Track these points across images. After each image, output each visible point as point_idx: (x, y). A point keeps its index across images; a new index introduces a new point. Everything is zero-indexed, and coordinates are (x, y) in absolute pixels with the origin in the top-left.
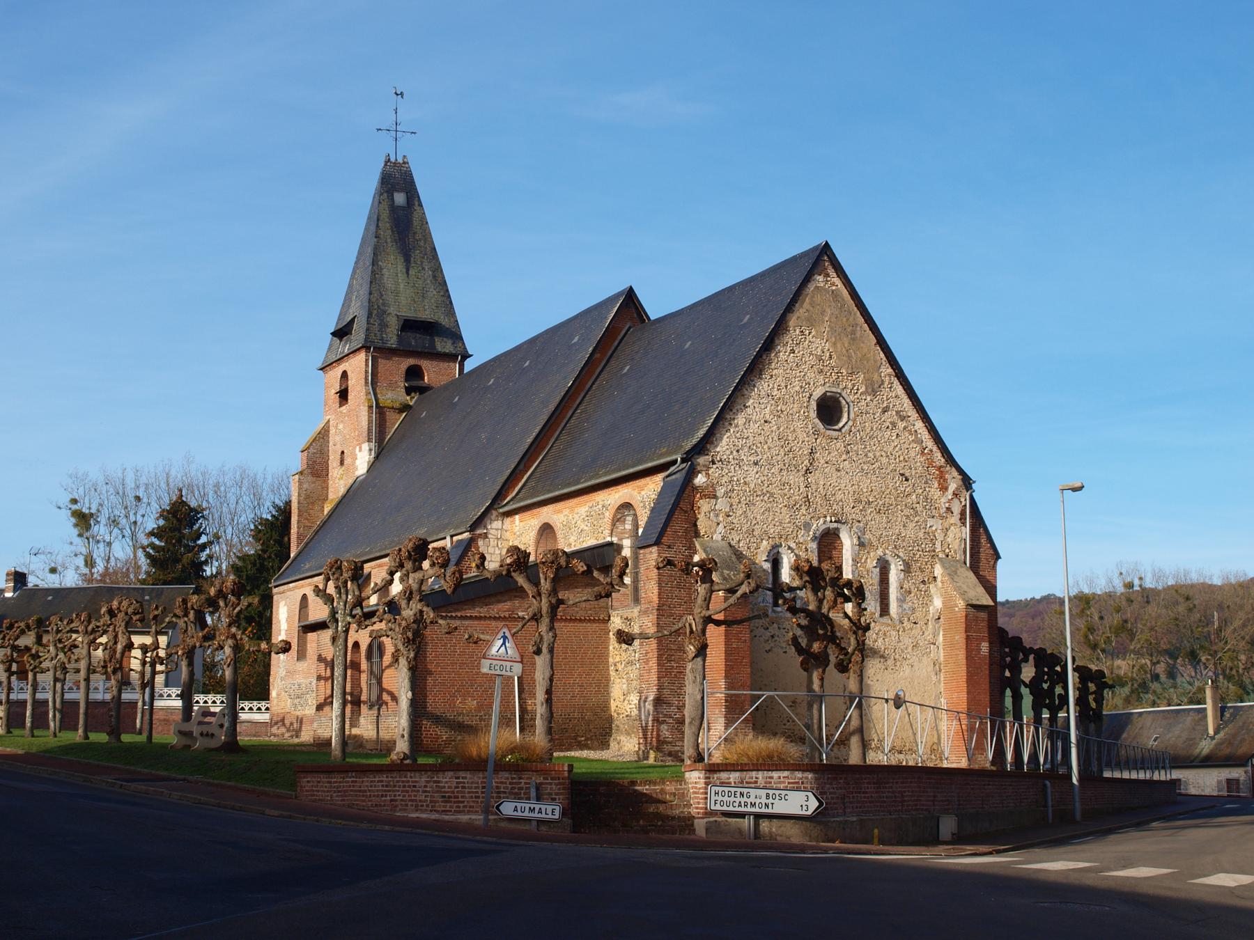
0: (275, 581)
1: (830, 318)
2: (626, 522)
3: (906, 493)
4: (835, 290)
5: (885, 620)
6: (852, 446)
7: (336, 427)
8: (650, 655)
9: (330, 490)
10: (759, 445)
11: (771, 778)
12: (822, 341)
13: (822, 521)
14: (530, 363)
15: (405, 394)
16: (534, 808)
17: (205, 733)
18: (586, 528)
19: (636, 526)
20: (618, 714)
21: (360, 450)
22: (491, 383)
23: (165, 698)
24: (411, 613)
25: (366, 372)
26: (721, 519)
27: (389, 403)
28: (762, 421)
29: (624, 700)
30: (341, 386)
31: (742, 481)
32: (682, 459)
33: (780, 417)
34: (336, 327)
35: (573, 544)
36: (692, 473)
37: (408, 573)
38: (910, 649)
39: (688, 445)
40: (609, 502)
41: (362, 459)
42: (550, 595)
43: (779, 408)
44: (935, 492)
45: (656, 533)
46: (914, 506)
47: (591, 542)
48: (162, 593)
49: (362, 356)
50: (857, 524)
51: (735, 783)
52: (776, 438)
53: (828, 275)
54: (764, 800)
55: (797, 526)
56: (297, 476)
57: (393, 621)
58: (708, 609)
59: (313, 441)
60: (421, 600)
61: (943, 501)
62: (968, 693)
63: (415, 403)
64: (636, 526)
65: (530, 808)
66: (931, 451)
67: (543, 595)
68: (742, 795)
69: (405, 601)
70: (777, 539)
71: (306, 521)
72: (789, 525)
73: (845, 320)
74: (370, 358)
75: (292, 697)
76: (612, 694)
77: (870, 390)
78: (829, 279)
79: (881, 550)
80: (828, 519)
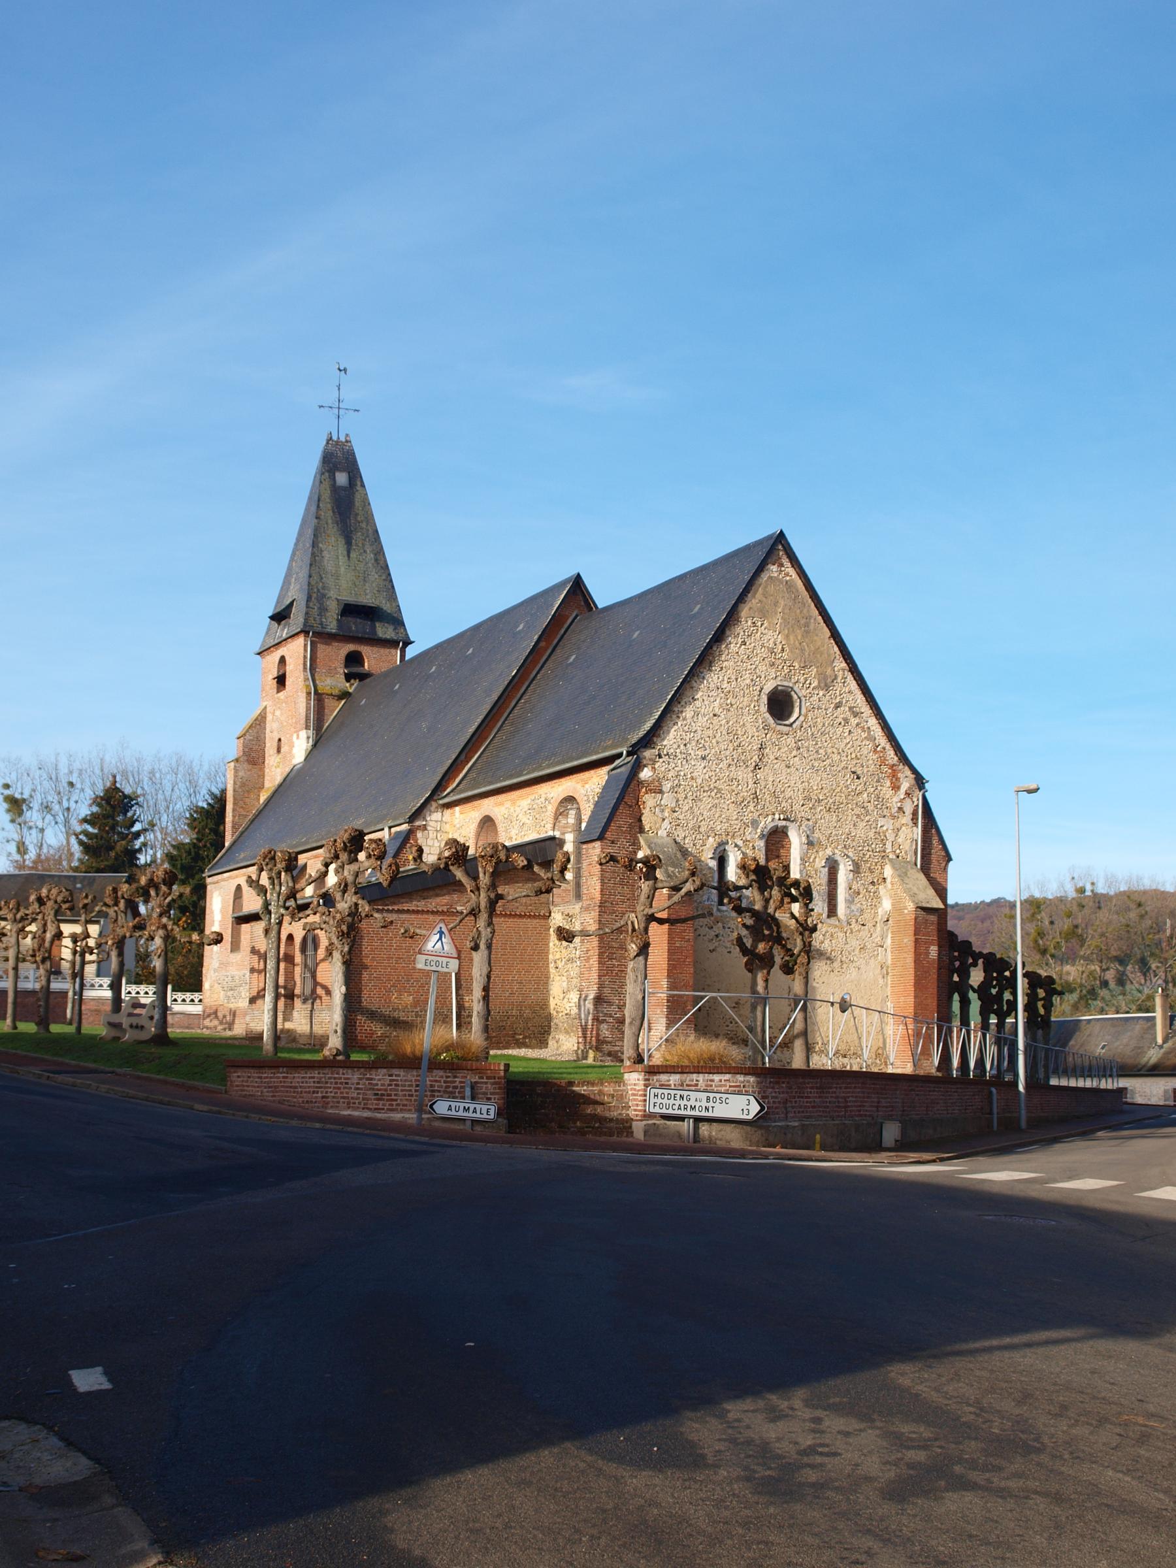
1: (783, 609)
3: (857, 792)
4: (789, 580)
5: (833, 921)
6: (803, 742)
8: (591, 953)
10: (707, 739)
13: (770, 818)
15: (344, 681)
16: (469, 1108)
17: (134, 1024)
19: (579, 820)
20: (557, 1012)
21: (298, 738)
22: (433, 670)
24: (346, 906)
25: (305, 657)
26: (666, 814)
28: (711, 715)
29: (564, 998)
30: (278, 671)
31: (689, 776)
32: (628, 752)
34: (275, 608)
36: (638, 766)
37: (344, 865)
38: (857, 952)
40: (552, 795)
41: (299, 747)
43: (729, 701)
46: (865, 805)
48: (94, 880)
50: (807, 822)
51: (675, 1085)
52: (724, 732)
53: (781, 565)
54: (704, 1104)
55: (744, 823)
56: (232, 764)
57: (327, 913)
59: (249, 728)
61: (895, 801)
62: (915, 997)
63: (355, 690)
64: (579, 820)
65: (464, 1107)
66: (884, 748)
67: (482, 890)
68: (682, 1097)
69: (340, 893)
70: (724, 836)
73: (798, 611)
75: (225, 989)
77: (822, 685)
78: (783, 569)
80: (777, 816)
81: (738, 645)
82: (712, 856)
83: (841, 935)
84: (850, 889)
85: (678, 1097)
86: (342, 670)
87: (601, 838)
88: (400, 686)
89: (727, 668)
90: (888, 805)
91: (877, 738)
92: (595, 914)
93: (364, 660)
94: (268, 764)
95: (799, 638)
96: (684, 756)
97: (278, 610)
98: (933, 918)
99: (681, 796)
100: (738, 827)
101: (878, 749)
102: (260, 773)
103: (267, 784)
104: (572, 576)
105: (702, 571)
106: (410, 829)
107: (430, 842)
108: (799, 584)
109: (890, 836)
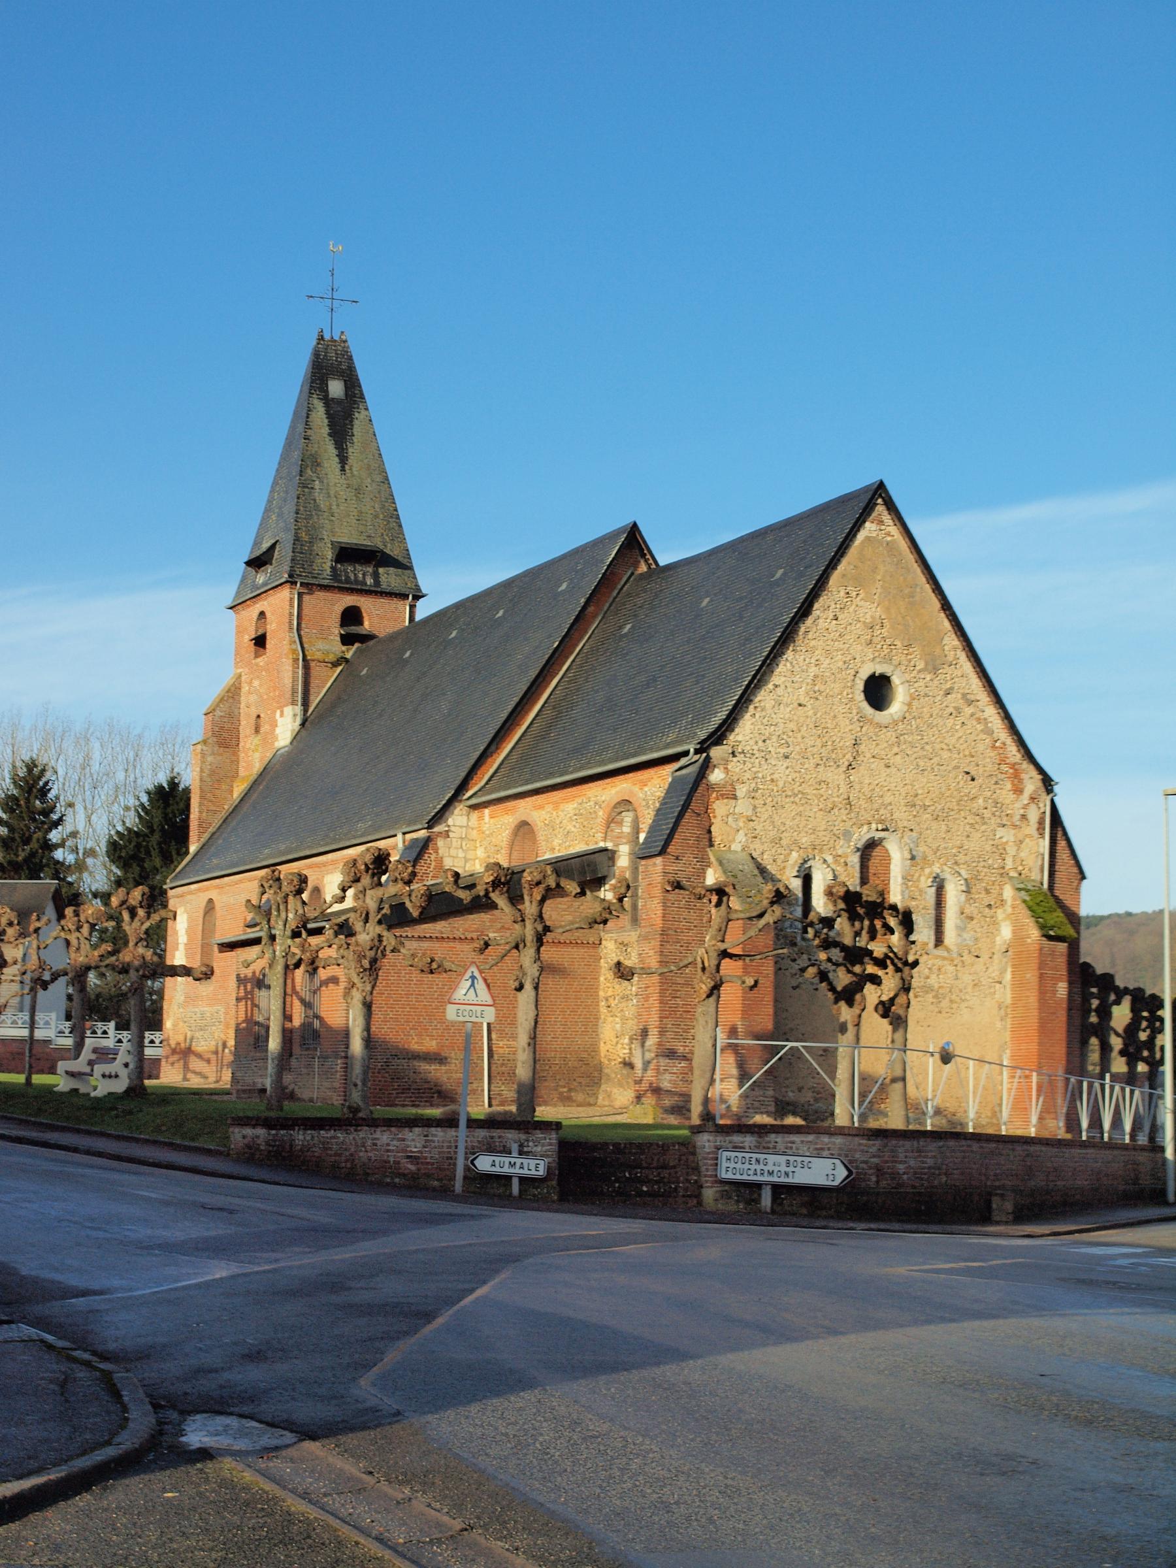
0: (171, 881)
2: (624, 824)
3: (972, 796)
4: (891, 541)
5: (940, 952)
7: (250, 683)
8: (650, 990)
9: (242, 764)
10: (791, 734)
11: (793, 1142)
12: (872, 606)
13: (865, 828)
14: (504, 613)
15: (340, 644)
17: (107, 1073)
18: (573, 829)
19: (636, 830)
20: (609, 1060)
21: (282, 715)
22: (453, 635)
23: (99, 1035)
24: (368, 938)
25: (291, 614)
26: (741, 824)
27: (318, 655)
28: (796, 704)
29: (617, 1043)
30: (257, 631)
31: (769, 778)
32: (695, 749)
33: (817, 699)
34: (251, 552)
35: (557, 848)
36: (706, 766)
38: (969, 989)
39: (702, 734)
40: (603, 798)
42: (536, 920)
43: (816, 688)
44: (1005, 793)
45: (660, 841)
47: (579, 847)
48: (15, 889)
49: (285, 593)
50: (910, 833)
52: (812, 726)
53: (881, 522)
54: (784, 1168)
55: (834, 835)
56: (199, 747)
57: (345, 946)
58: (723, 941)
60: (380, 922)
61: (1017, 810)
62: (1040, 1044)
63: (353, 655)
64: (636, 830)
66: (1004, 744)
67: (528, 922)
69: (361, 923)
70: (810, 850)
71: (210, 804)
72: (824, 833)
73: (902, 578)
74: (296, 596)
75: (193, 1028)
76: (602, 1036)
77: (930, 667)
78: (883, 527)
79: (938, 865)
80: (874, 826)
81: (828, 621)
82: (796, 874)
83: (951, 968)
84: (962, 913)
85: (753, 1161)
86: (336, 631)
87: (662, 852)
88: (411, 655)
89: (814, 648)
90: (1008, 812)
91: (996, 731)
92: (656, 943)
93: (363, 617)
94: (243, 747)
95: (902, 611)
96: (763, 754)
97: (258, 553)
98: (1062, 947)
99: (759, 802)
100: (827, 839)
101: (997, 744)
102: (234, 758)
103: (242, 772)
104: (627, 525)
105: (786, 526)
106: (429, 837)
107: (453, 852)
108: (903, 545)
109: (1011, 850)
